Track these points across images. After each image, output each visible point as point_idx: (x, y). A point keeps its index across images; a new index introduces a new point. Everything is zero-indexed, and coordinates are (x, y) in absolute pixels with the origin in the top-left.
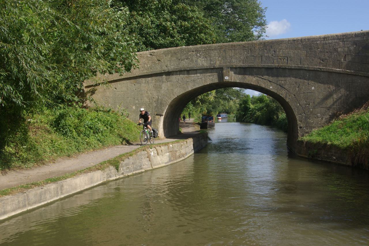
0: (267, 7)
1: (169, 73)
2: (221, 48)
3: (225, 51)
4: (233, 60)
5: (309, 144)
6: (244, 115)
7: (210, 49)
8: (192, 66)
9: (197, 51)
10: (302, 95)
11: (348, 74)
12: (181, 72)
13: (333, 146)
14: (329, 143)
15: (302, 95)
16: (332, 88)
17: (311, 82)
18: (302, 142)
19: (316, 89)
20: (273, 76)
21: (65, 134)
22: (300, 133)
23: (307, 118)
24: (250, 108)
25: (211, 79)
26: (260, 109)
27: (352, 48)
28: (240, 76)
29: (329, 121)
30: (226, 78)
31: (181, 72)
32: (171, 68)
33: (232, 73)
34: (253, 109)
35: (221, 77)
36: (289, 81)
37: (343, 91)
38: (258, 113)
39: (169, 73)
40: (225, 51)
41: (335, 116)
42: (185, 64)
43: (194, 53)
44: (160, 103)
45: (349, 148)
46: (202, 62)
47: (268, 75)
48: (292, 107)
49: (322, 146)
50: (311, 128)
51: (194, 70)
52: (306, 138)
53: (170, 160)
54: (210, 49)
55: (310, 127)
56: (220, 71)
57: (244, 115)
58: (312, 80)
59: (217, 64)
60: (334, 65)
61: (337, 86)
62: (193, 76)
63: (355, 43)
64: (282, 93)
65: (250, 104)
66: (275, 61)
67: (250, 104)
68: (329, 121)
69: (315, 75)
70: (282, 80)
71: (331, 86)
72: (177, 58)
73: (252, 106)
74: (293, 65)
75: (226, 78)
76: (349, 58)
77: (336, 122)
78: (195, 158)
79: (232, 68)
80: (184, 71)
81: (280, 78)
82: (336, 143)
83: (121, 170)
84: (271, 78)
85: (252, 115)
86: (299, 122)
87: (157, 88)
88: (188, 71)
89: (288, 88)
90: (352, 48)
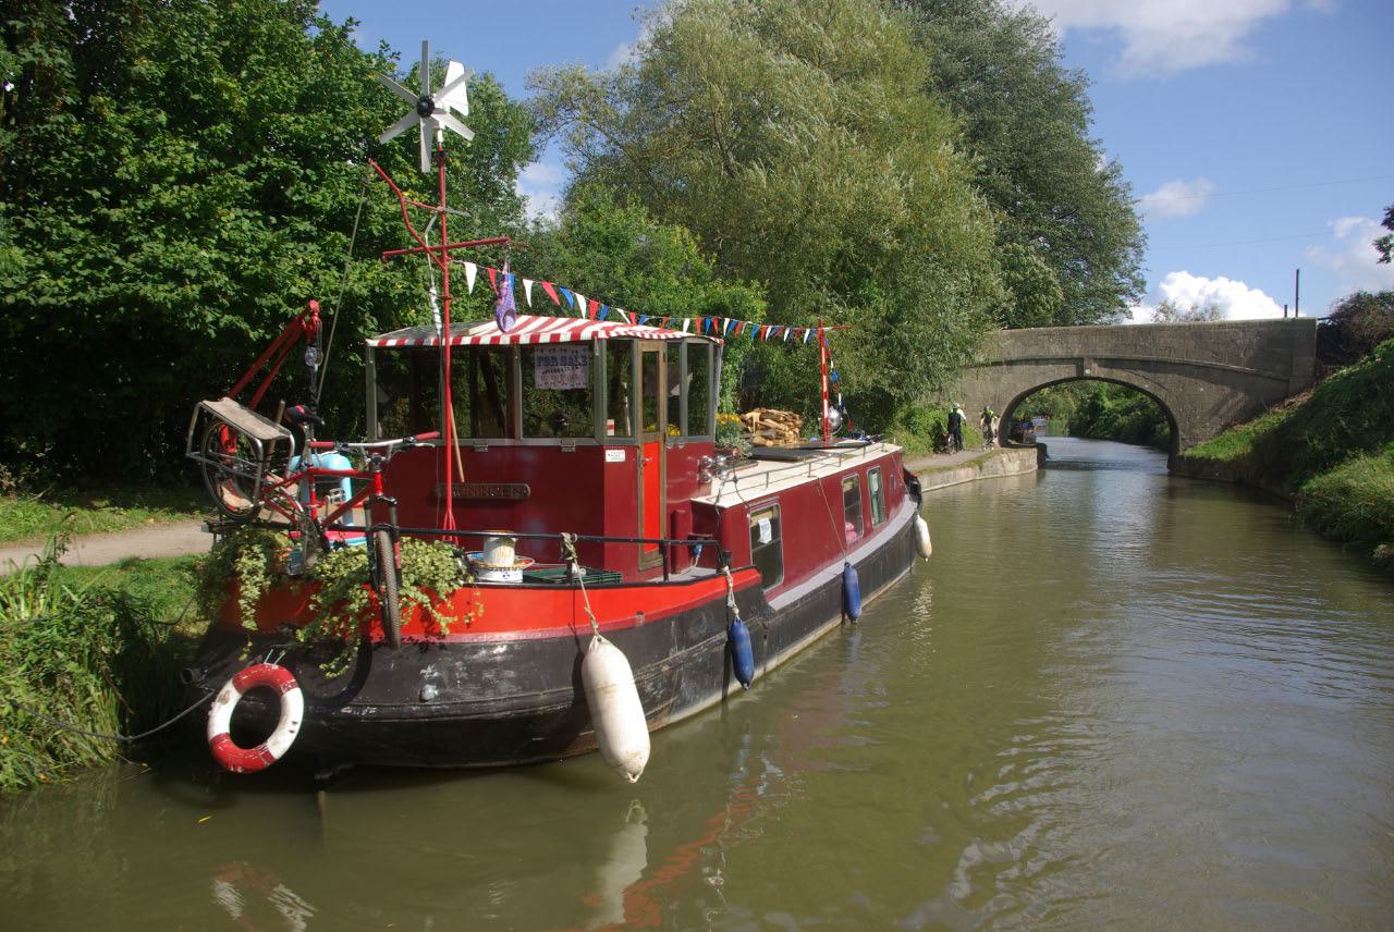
0: (1100, 137)
1: (1010, 363)
2: (1082, 332)
3: (1087, 336)
4: (1097, 349)
5: (1191, 459)
6: (1090, 423)
7: (1067, 332)
8: (1043, 354)
9: (1050, 335)
10: (1186, 397)
11: (1246, 373)
12: (1027, 361)
13: (1217, 460)
14: (1213, 457)
15: (1186, 397)
16: (1227, 390)
17: (1200, 382)
18: (1182, 457)
19: (1207, 393)
20: (1150, 371)
21: (914, 433)
22: (1181, 447)
23: (1193, 426)
24: (1103, 408)
25: (1068, 371)
26: (1127, 411)
27: (1255, 340)
28: (1106, 370)
29: (1220, 433)
30: (1087, 372)
31: (1027, 361)
32: (1015, 355)
33: (1095, 365)
34: (1111, 411)
35: (1080, 369)
36: (1170, 379)
37: (1241, 395)
38: (1123, 420)
39: (1010, 363)
40: (1087, 336)
41: (1227, 426)
42: (1033, 352)
43: (1046, 338)
44: (997, 401)
45: (1233, 461)
46: (1056, 350)
47: (1142, 369)
48: (1174, 413)
49: (1206, 462)
50: (1197, 440)
51: (1044, 360)
52: (1189, 452)
53: (1021, 470)
54: (1067, 332)
55: (1195, 439)
56: (1079, 362)
57: (1090, 423)
58: (1201, 378)
59: (1076, 353)
60: (1232, 362)
61: (1234, 387)
62: (1042, 367)
63: (1259, 334)
64: (1161, 395)
65: (1105, 399)
66: (1153, 352)
67: (1105, 399)
68: (1220, 433)
69: (1204, 372)
70: (1161, 377)
71: (1225, 387)
72: (1023, 344)
73: (1108, 404)
74: (1175, 358)
75: (1087, 372)
76: (1251, 353)
77: (1228, 433)
78: (1038, 474)
79: (1096, 360)
80: (1032, 360)
81: (1159, 375)
82: (1220, 456)
83: (984, 470)
84: (1147, 375)
85: (1108, 423)
86: (1181, 433)
87: (996, 380)
88: (1037, 361)
89: (1168, 388)
90: (1255, 340)
